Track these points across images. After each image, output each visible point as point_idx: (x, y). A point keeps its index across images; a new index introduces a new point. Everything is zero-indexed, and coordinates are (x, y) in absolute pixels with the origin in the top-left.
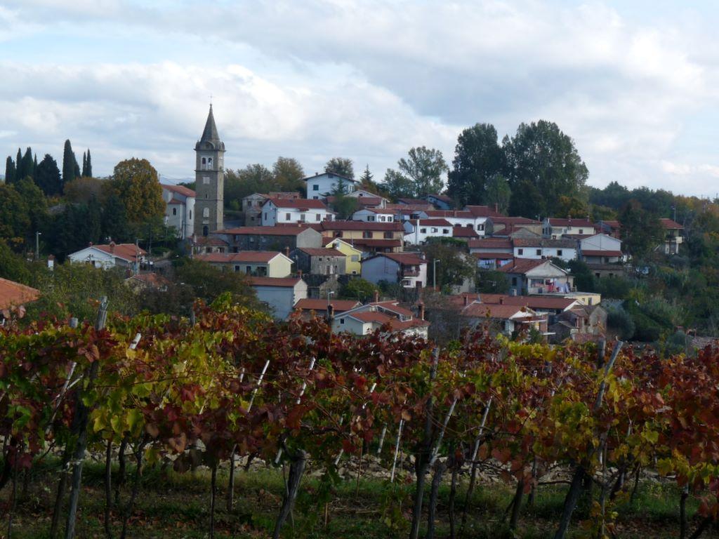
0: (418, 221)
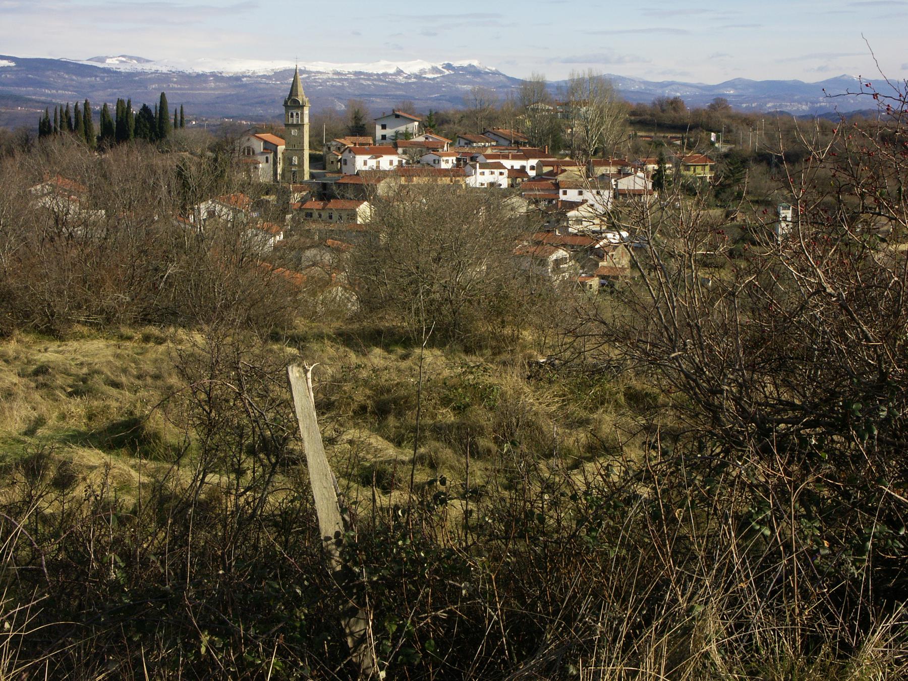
0: (478, 165)
